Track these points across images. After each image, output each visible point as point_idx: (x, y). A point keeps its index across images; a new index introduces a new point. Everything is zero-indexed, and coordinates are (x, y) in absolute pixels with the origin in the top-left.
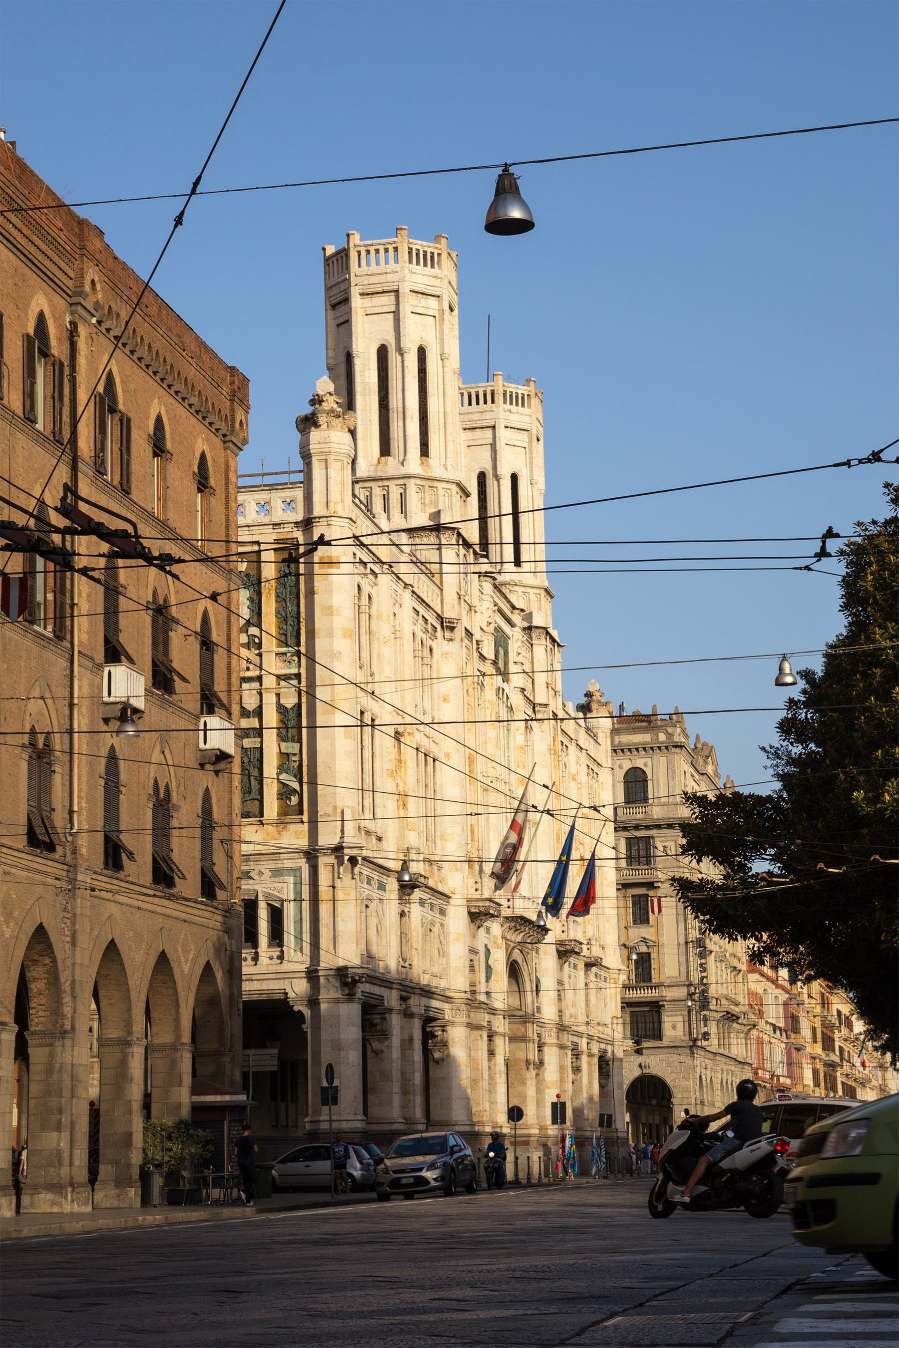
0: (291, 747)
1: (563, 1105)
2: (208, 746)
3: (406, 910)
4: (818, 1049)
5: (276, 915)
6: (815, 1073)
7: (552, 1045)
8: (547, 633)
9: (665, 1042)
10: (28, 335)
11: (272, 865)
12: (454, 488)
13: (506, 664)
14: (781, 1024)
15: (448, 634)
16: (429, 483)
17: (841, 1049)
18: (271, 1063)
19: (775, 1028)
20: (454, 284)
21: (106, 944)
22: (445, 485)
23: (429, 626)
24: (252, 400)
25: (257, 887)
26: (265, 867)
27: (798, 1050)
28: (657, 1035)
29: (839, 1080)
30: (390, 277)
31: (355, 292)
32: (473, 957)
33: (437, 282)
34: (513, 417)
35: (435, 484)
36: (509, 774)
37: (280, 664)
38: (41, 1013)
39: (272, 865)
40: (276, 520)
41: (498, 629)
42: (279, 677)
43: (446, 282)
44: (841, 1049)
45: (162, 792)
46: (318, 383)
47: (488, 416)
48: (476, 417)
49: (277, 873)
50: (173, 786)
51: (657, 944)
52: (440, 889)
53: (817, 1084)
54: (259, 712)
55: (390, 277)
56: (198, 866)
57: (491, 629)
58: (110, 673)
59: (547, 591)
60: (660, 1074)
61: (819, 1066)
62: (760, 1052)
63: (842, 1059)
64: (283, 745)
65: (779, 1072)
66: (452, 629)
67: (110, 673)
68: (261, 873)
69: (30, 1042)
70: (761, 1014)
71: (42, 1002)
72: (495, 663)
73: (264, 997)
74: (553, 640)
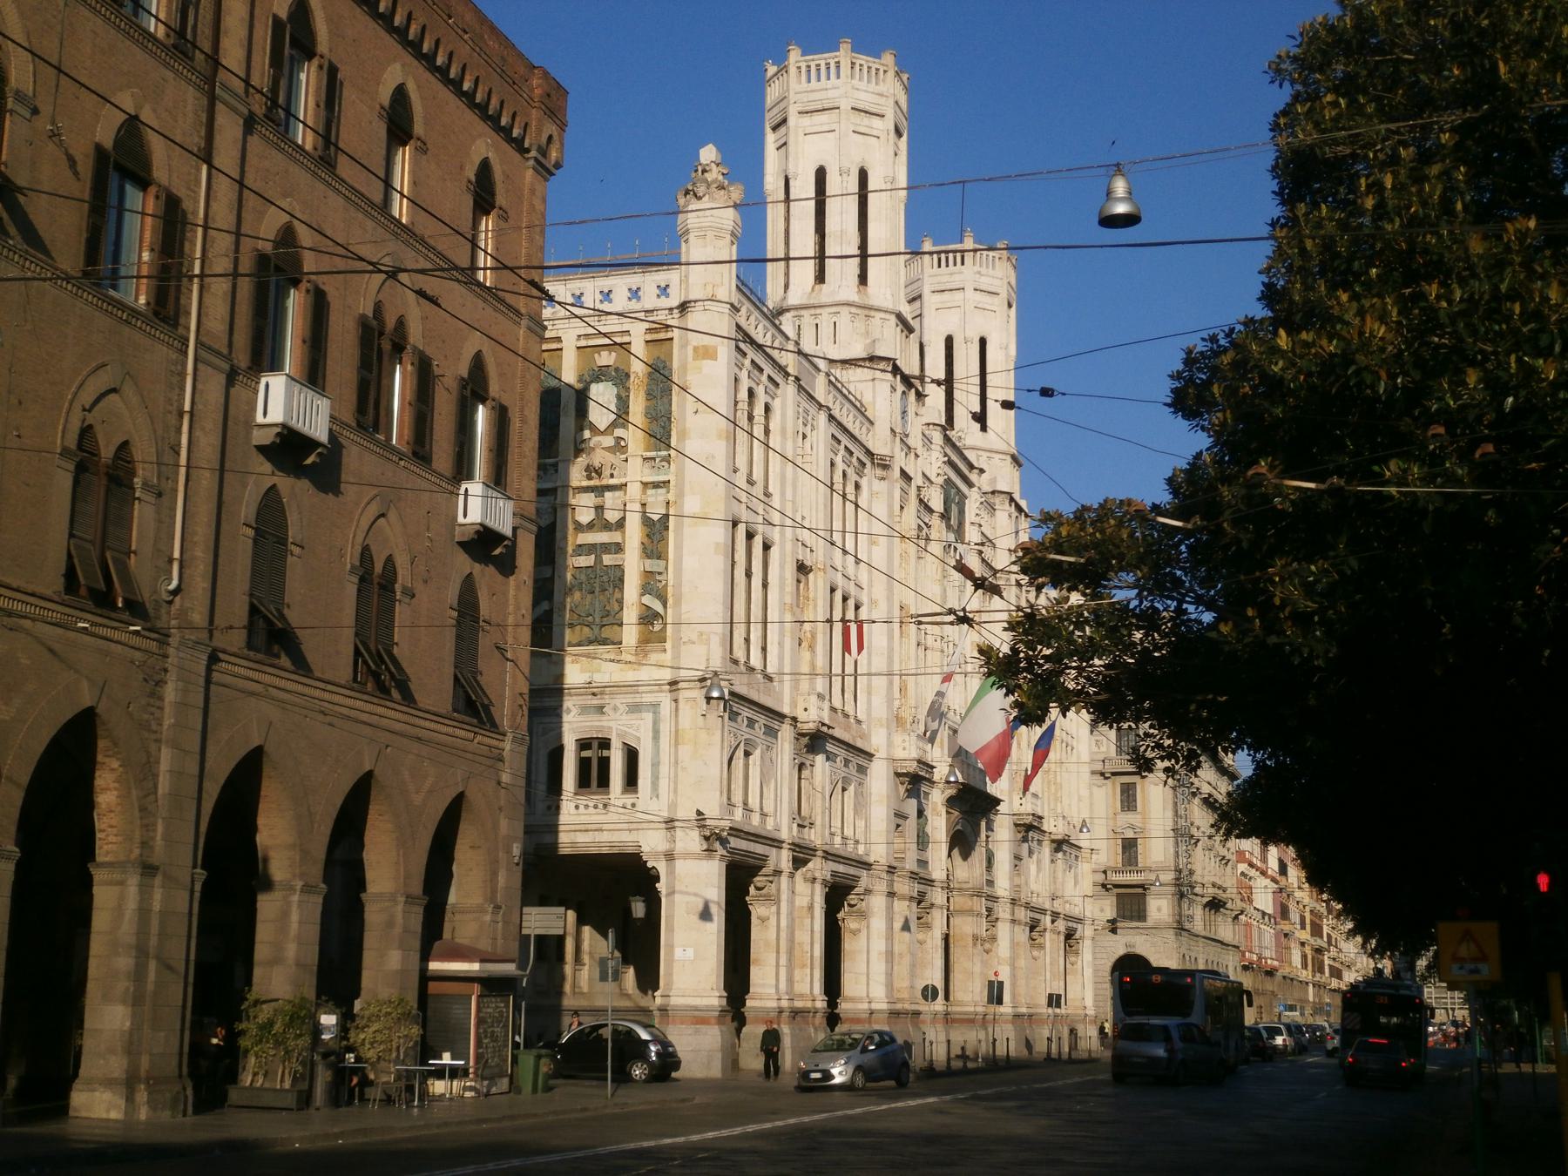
0: (651, 565)
1: (1001, 984)
2: (469, 520)
3: (808, 763)
4: (1305, 935)
5: (632, 756)
6: (1304, 957)
7: (1004, 920)
8: (1012, 500)
9: (1150, 922)
10: (276, 18)
11: (630, 699)
12: (893, 318)
13: (961, 524)
14: (1270, 911)
15: (879, 472)
16: (866, 312)
17: (1329, 936)
18: (555, 924)
19: (1264, 914)
20: (904, 106)
21: (243, 752)
22: (882, 315)
23: (854, 460)
24: (571, 117)
25: (611, 724)
26: (621, 701)
27: (1286, 935)
28: (1141, 915)
29: (1327, 962)
30: (831, 94)
31: (792, 112)
32: (900, 821)
33: (882, 101)
34: (983, 279)
35: (872, 313)
36: (870, 573)
37: (647, 471)
38: (112, 839)
39: (630, 699)
40: (649, 306)
41: (948, 482)
42: (645, 485)
43: (891, 102)
44: (1329, 936)
45: (378, 568)
46: (702, 152)
47: (957, 277)
48: (946, 279)
49: (635, 708)
50: (402, 562)
51: (1143, 830)
52: (859, 744)
53: (1305, 966)
54: (620, 524)
55: (831, 94)
56: (449, 670)
57: (940, 480)
58: (267, 385)
59: (1014, 457)
60: (1144, 954)
61: (1308, 950)
62: (1248, 937)
63: (1329, 943)
64: (648, 562)
65: (1267, 953)
66: (885, 467)
67: (267, 385)
68: (615, 709)
69: (96, 878)
70: (1250, 901)
71: (113, 822)
72: (945, 516)
73: (615, 850)
74: (1019, 509)
